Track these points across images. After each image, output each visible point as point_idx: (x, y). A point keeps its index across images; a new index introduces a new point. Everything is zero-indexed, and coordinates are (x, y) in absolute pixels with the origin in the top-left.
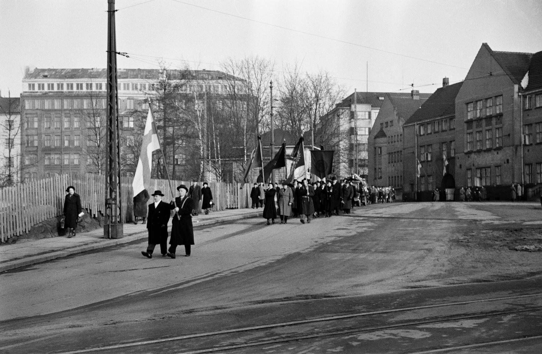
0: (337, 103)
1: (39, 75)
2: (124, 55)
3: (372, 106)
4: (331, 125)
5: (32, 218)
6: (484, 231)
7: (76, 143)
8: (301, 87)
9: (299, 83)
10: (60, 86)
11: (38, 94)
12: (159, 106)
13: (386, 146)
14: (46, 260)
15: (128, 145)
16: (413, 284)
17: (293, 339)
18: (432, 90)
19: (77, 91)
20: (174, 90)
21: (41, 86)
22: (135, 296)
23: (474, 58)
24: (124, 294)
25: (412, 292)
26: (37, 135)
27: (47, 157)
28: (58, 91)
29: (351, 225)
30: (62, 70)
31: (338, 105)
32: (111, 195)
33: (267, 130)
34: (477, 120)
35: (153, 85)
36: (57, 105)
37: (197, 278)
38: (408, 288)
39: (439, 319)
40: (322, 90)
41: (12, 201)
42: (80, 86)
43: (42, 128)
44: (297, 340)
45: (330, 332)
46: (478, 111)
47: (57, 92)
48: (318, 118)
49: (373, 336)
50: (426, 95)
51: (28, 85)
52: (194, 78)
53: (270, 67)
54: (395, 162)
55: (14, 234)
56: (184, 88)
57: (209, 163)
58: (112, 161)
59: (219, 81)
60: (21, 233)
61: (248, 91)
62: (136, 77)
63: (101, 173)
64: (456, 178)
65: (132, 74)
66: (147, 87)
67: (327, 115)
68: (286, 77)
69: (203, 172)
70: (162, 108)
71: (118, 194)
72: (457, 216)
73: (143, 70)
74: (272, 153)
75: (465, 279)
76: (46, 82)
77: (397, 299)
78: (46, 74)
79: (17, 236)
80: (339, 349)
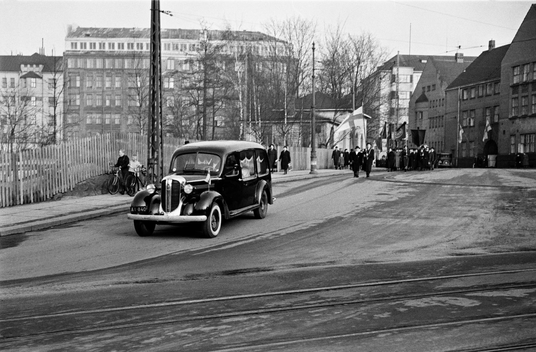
0: (380, 66)
1: (81, 34)
2: (168, 14)
3: (414, 70)
4: (372, 89)
5: (76, 175)
6: (530, 199)
7: (117, 103)
8: (343, 49)
9: (341, 46)
10: (102, 45)
11: (80, 53)
12: (200, 67)
13: (427, 111)
14: (90, 217)
15: (168, 106)
16: (458, 251)
17: (339, 303)
18: (477, 53)
19: (119, 50)
20: (215, 50)
21: (83, 45)
22: (178, 256)
23: (523, 20)
24: (168, 253)
25: (458, 260)
26: (79, 94)
27: (88, 117)
28: (100, 50)
29: (392, 190)
30: (104, 29)
31: (379, 68)
32: (153, 154)
33: (307, 93)
34: (524, 85)
35: (194, 45)
36: (99, 64)
37: (239, 240)
38: (453, 255)
39: (488, 288)
40: (364, 53)
41: (57, 158)
42: (121, 46)
43: (84, 87)
44: (342, 304)
45: (375, 297)
46: (525, 75)
47: (98, 51)
48: (359, 81)
49: (420, 303)
50: (470, 58)
51: (70, 44)
52: (235, 39)
53: (312, 28)
54: (436, 127)
55: (59, 191)
56: (224, 49)
57: (249, 125)
58: (155, 121)
59: (260, 42)
60: (66, 191)
61: (289, 53)
62: (176, 37)
63: (143, 133)
64: (499, 145)
65: (173, 34)
66: (188, 47)
67: (368, 78)
68: (328, 37)
69: (243, 134)
70: (202, 68)
71: (160, 154)
72: (500, 183)
73: (184, 30)
74: (312, 116)
75: (504, 248)
76: (88, 41)
77: (443, 266)
78: (88, 33)
79: (61, 193)
80: (386, 315)
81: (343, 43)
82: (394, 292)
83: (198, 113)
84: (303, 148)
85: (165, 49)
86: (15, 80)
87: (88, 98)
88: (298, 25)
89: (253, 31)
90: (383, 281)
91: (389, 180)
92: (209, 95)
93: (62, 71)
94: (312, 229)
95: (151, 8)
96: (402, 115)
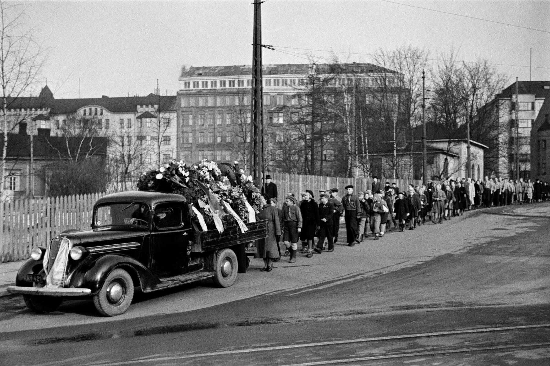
0: (497, 93)
2: (269, 48)
3: (536, 97)
4: (490, 117)
7: (228, 140)
8: (457, 77)
9: (455, 74)
10: (214, 83)
11: (193, 91)
17: (440, 352)
30: (216, 67)
31: (498, 96)
33: (419, 123)
45: (483, 347)
53: (424, 57)
59: (369, 74)
66: (297, 82)
67: (484, 107)
69: (351, 168)
70: (311, 103)
73: (293, 65)
74: (423, 147)
78: (201, 72)
81: (457, 70)
82: (503, 341)
83: (307, 147)
84: (414, 181)
85: (266, 85)
86: (132, 120)
87: (200, 136)
88: (409, 55)
89: (361, 63)
90: (493, 327)
91: (507, 213)
92: (317, 129)
93: (176, 110)
94: (417, 268)
95: (252, 43)
96: (523, 145)
